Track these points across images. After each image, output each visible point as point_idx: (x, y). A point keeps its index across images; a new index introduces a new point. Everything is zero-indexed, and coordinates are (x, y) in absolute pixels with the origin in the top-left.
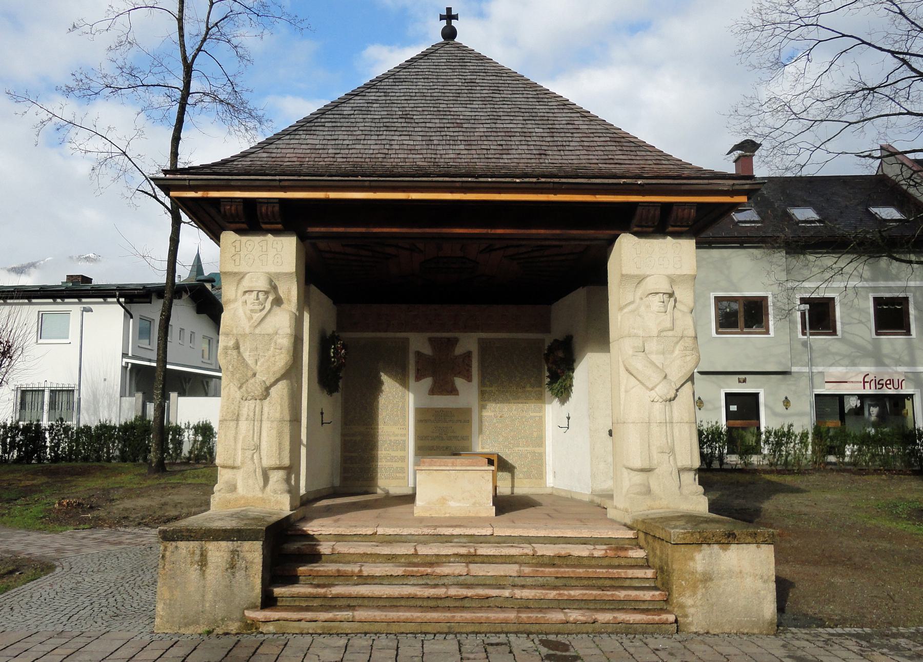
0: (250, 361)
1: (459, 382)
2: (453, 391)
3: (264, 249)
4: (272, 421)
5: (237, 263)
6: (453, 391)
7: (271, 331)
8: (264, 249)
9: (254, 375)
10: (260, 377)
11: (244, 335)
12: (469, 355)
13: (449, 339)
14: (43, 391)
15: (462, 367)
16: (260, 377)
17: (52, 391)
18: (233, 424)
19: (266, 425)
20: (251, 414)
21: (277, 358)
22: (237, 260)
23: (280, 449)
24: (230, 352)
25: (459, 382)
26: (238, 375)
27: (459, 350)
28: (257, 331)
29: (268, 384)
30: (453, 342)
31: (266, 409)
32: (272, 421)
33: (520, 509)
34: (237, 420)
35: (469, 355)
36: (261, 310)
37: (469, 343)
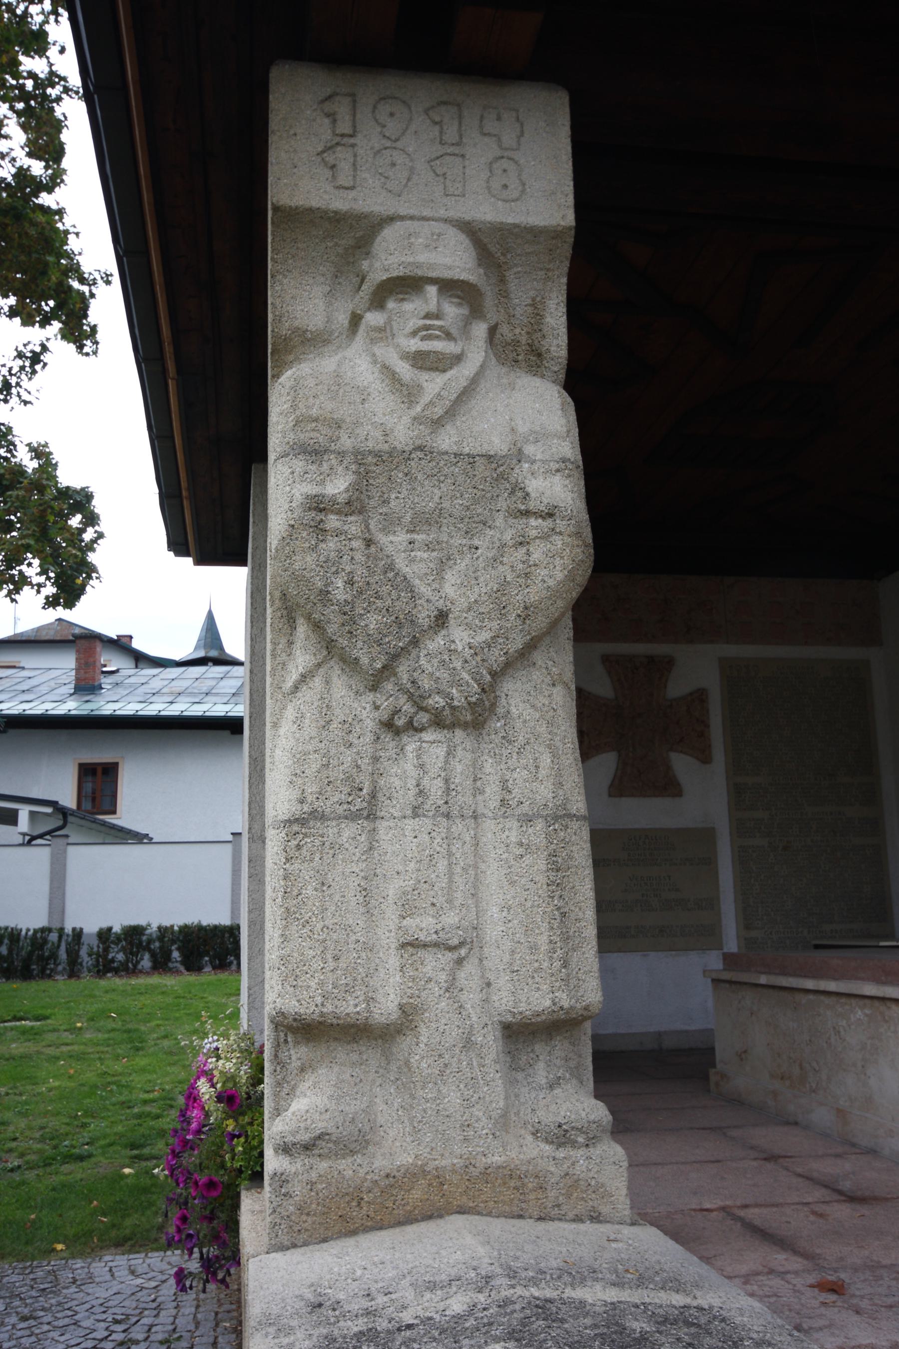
1: (681, 764)
2: (669, 787)
4: (527, 820)
5: (342, 180)
6: (669, 787)
7: (498, 444)
12: (700, 697)
13: (651, 659)
15: (684, 726)
25: (681, 764)
27: (677, 687)
28: (446, 440)
30: (662, 667)
34: (372, 816)
35: (700, 697)
37: (697, 668)
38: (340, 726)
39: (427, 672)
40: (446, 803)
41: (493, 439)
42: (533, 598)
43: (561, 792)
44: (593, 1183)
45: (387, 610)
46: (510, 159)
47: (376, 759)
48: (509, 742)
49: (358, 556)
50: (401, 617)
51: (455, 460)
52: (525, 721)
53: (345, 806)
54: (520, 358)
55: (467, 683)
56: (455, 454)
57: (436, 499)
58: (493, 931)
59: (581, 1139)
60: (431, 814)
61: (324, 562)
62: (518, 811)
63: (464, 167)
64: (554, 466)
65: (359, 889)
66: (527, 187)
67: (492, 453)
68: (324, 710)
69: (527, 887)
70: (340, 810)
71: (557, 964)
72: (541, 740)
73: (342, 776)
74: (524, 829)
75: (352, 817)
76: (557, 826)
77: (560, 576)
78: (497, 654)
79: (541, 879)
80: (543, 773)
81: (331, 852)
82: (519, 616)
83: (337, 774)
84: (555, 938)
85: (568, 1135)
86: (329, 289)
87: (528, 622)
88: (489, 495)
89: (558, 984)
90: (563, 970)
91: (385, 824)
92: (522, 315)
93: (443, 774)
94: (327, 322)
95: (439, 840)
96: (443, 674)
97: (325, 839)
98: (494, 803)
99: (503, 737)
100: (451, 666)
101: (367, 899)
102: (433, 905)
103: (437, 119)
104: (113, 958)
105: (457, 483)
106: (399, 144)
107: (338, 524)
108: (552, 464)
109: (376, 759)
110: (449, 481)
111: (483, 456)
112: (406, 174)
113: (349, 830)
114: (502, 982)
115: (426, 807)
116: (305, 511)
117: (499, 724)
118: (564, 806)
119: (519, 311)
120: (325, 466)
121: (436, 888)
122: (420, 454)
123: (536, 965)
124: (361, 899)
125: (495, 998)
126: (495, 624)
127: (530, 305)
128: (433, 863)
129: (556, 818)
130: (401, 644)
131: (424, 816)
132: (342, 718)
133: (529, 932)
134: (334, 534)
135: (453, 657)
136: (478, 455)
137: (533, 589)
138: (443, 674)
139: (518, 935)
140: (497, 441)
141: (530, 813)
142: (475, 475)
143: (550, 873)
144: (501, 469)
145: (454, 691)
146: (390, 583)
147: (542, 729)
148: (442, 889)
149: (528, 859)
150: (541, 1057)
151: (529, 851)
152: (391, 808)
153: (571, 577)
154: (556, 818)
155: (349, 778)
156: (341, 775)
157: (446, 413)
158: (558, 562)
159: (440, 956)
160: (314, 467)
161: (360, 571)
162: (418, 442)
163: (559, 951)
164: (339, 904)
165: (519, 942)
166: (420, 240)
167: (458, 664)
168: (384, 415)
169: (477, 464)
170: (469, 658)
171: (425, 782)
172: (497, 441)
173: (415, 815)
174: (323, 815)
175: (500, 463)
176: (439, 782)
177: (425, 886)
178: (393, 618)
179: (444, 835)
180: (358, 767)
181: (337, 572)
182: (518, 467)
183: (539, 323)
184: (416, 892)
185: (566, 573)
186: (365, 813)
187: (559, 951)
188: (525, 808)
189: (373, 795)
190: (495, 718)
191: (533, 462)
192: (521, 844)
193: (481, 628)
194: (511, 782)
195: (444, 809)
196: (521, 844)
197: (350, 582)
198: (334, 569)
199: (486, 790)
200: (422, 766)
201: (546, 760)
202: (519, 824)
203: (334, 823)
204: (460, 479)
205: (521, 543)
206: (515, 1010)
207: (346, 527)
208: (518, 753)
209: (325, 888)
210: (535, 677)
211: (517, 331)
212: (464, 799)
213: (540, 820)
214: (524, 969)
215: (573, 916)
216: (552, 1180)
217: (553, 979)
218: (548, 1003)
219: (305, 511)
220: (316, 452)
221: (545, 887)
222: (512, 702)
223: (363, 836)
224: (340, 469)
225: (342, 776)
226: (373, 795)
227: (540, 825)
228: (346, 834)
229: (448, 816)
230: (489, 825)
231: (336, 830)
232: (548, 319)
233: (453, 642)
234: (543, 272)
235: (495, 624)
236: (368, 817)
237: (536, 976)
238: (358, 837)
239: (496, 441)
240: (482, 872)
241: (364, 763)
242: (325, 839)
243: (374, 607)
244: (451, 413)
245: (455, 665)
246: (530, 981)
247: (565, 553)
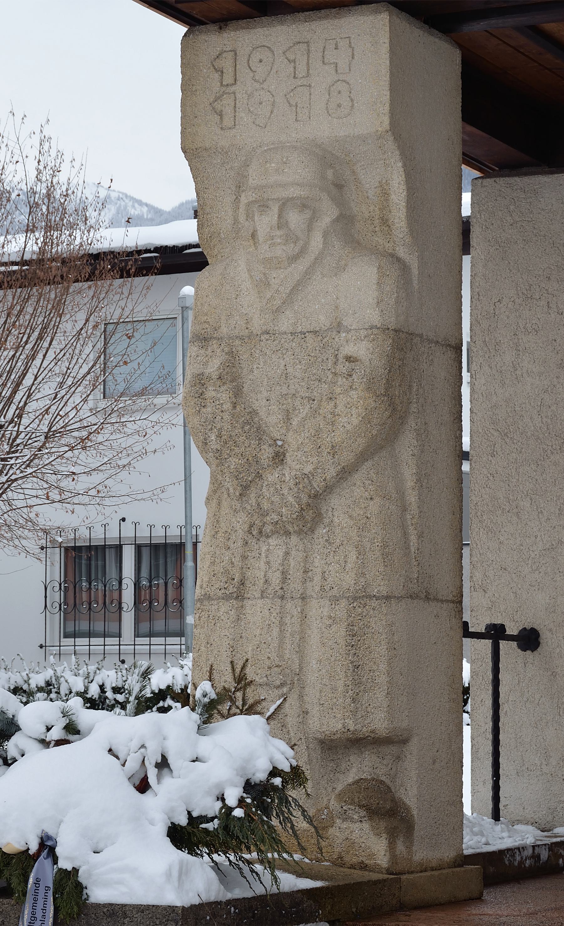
0: (271, 418)
3: (301, 70)
4: (335, 600)
5: (228, 121)
7: (323, 321)
8: (301, 70)
9: (279, 458)
10: (297, 463)
11: (250, 338)
14: (119, 548)
16: (297, 463)
17: (139, 548)
18: (224, 609)
19: (319, 610)
20: (275, 578)
21: (341, 401)
22: (228, 111)
23: (357, 683)
24: (210, 393)
26: (234, 462)
28: (285, 324)
29: (318, 484)
31: (318, 562)
32: (335, 600)
33: (393, 89)
34: (240, 596)
36: (294, 258)
38: (223, 535)
39: (266, 498)
40: (282, 588)
41: (320, 317)
42: (338, 439)
43: (362, 580)
44: (363, 845)
45: (242, 455)
46: (344, 81)
47: (244, 558)
48: (330, 543)
49: (226, 416)
50: (250, 459)
51: (292, 338)
52: (342, 528)
53: (223, 591)
54: (377, 229)
55: (291, 504)
56: (291, 333)
57: (282, 367)
58: (314, 675)
59: (356, 817)
60: (271, 596)
61: (204, 422)
62: (330, 594)
63: (310, 94)
64: (363, 333)
65: (229, 647)
66: (355, 102)
67: (318, 329)
68: (215, 524)
69: (333, 647)
70: (220, 593)
71: (349, 700)
72: (351, 542)
73: (222, 570)
74: (333, 606)
75: (227, 598)
76: (355, 604)
77: (355, 421)
78: (318, 480)
79: (342, 642)
80: (349, 565)
81: (213, 622)
82: (329, 453)
83: (219, 569)
84: (349, 683)
85: (347, 814)
86: (235, 197)
87: (336, 457)
88: (319, 360)
89: (347, 714)
90: (352, 705)
91: (250, 602)
92: (374, 196)
93: (281, 568)
94: (234, 223)
95: (275, 614)
96: (276, 499)
97: (210, 613)
98: (317, 588)
99: (327, 540)
100: (281, 492)
101: (234, 653)
102: (269, 658)
103: (292, 57)
104: (151, 693)
105: (296, 354)
106: (265, 86)
107: (214, 394)
108: (362, 331)
109: (244, 558)
110: (290, 353)
111: (311, 332)
112: (269, 108)
113: (224, 607)
114: (315, 711)
115: (269, 591)
116: (192, 386)
117: (324, 531)
118: (364, 588)
119: (371, 193)
120: (209, 352)
121: (270, 647)
122: (267, 336)
123: (335, 700)
124: (230, 653)
125: (311, 722)
126: (315, 460)
127: (379, 187)
128: (270, 629)
129: (355, 599)
130: (250, 479)
131: (267, 597)
132: (225, 529)
133: (332, 678)
134: (212, 401)
135: (283, 487)
136: (308, 332)
137: (337, 433)
138: (276, 499)
139: (324, 680)
140: (323, 318)
141: (338, 595)
142: (307, 347)
143: (348, 637)
144: (325, 340)
145: (284, 510)
146: (244, 435)
147: (353, 534)
148: (275, 647)
149: (334, 628)
150: (354, 765)
151: (335, 621)
152: (254, 591)
153: (366, 420)
154: (355, 599)
155: (227, 572)
156: (222, 569)
157: (284, 303)
158: (354, 411)
159: (270, 692)
160: (202, 351)
161: (227, 426)
162: (264, 328)
163: (350, 692)
164: (216, 656)
165: (325, 685)
166: (273, 165)
167: (285, 491)
168: (248, 307)
169: (308, 338)
170: (292, 486)
171: (270, 574)
172: (323, 318)
173: (262, 597)
174: (209, 597)
175: (324, 335)
176: (278, 574)
177: (264, 645)
178: (245, 460)
179: (278, 611)
180: (232, 563)
181: (211, 429)
182: (337, 337)
183: (387, 200)
184: (259, 649)
185: (361, 419)
186: (235, 595)
187: (350, 692)
188: (335, 592)
189: (242, 583)
190: (323, 526)
191: (348, 331)
192: (330, 617)
193: (307, 462)
194: (327, 573)
195: (280, 592)
196: (330, 617)
197: (219, 436)
198: (210, 427)
199: (315, 578)
200: (268, 563)
201: (353, 556)
202: (330, 603)
203: (216, 602)
204: (297, 350)
205: (331, 398)
206: (321, 730)
207: (219, 395)
208: (334, 552)
209: (209, 646)
210: (356, 494)
211: (371, 208)
212: (295, 585)
213: (344, 600)
214: (327, 703)
215: (367, 668)
216: (338, 842)
217: (345, 710)
218: (340, 726)
219: (192, 386)
220: (205, 339)
221: (344, 647)
222: (336, 514)
223: (233, 611)
224: (218, 351)
225: (222, 570)
226: (242, 583)
227: (344, 603)
228: (223, 609)
229: (282, 598)
230: (314, 603)
231: (216, 607)
232: (393, 196)
233: (284, 475)
234: (382, 162)
235: (315, 460)
236: (237, 598)
237: (334, 708)
238: (230, 612)
239: (322, 318)
240: (308, 636)
241: (237, 560)
242: (210, 613)
243: (234, 453)
244: (289, 300)
245: (283, 492)
246: (330, 711)
247: (359, 404)
